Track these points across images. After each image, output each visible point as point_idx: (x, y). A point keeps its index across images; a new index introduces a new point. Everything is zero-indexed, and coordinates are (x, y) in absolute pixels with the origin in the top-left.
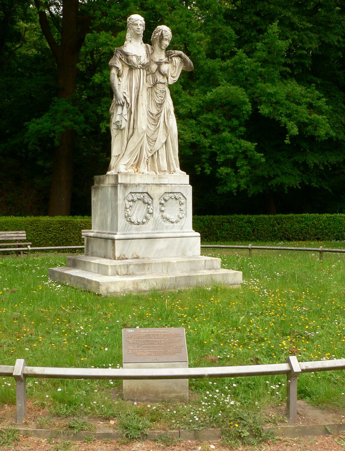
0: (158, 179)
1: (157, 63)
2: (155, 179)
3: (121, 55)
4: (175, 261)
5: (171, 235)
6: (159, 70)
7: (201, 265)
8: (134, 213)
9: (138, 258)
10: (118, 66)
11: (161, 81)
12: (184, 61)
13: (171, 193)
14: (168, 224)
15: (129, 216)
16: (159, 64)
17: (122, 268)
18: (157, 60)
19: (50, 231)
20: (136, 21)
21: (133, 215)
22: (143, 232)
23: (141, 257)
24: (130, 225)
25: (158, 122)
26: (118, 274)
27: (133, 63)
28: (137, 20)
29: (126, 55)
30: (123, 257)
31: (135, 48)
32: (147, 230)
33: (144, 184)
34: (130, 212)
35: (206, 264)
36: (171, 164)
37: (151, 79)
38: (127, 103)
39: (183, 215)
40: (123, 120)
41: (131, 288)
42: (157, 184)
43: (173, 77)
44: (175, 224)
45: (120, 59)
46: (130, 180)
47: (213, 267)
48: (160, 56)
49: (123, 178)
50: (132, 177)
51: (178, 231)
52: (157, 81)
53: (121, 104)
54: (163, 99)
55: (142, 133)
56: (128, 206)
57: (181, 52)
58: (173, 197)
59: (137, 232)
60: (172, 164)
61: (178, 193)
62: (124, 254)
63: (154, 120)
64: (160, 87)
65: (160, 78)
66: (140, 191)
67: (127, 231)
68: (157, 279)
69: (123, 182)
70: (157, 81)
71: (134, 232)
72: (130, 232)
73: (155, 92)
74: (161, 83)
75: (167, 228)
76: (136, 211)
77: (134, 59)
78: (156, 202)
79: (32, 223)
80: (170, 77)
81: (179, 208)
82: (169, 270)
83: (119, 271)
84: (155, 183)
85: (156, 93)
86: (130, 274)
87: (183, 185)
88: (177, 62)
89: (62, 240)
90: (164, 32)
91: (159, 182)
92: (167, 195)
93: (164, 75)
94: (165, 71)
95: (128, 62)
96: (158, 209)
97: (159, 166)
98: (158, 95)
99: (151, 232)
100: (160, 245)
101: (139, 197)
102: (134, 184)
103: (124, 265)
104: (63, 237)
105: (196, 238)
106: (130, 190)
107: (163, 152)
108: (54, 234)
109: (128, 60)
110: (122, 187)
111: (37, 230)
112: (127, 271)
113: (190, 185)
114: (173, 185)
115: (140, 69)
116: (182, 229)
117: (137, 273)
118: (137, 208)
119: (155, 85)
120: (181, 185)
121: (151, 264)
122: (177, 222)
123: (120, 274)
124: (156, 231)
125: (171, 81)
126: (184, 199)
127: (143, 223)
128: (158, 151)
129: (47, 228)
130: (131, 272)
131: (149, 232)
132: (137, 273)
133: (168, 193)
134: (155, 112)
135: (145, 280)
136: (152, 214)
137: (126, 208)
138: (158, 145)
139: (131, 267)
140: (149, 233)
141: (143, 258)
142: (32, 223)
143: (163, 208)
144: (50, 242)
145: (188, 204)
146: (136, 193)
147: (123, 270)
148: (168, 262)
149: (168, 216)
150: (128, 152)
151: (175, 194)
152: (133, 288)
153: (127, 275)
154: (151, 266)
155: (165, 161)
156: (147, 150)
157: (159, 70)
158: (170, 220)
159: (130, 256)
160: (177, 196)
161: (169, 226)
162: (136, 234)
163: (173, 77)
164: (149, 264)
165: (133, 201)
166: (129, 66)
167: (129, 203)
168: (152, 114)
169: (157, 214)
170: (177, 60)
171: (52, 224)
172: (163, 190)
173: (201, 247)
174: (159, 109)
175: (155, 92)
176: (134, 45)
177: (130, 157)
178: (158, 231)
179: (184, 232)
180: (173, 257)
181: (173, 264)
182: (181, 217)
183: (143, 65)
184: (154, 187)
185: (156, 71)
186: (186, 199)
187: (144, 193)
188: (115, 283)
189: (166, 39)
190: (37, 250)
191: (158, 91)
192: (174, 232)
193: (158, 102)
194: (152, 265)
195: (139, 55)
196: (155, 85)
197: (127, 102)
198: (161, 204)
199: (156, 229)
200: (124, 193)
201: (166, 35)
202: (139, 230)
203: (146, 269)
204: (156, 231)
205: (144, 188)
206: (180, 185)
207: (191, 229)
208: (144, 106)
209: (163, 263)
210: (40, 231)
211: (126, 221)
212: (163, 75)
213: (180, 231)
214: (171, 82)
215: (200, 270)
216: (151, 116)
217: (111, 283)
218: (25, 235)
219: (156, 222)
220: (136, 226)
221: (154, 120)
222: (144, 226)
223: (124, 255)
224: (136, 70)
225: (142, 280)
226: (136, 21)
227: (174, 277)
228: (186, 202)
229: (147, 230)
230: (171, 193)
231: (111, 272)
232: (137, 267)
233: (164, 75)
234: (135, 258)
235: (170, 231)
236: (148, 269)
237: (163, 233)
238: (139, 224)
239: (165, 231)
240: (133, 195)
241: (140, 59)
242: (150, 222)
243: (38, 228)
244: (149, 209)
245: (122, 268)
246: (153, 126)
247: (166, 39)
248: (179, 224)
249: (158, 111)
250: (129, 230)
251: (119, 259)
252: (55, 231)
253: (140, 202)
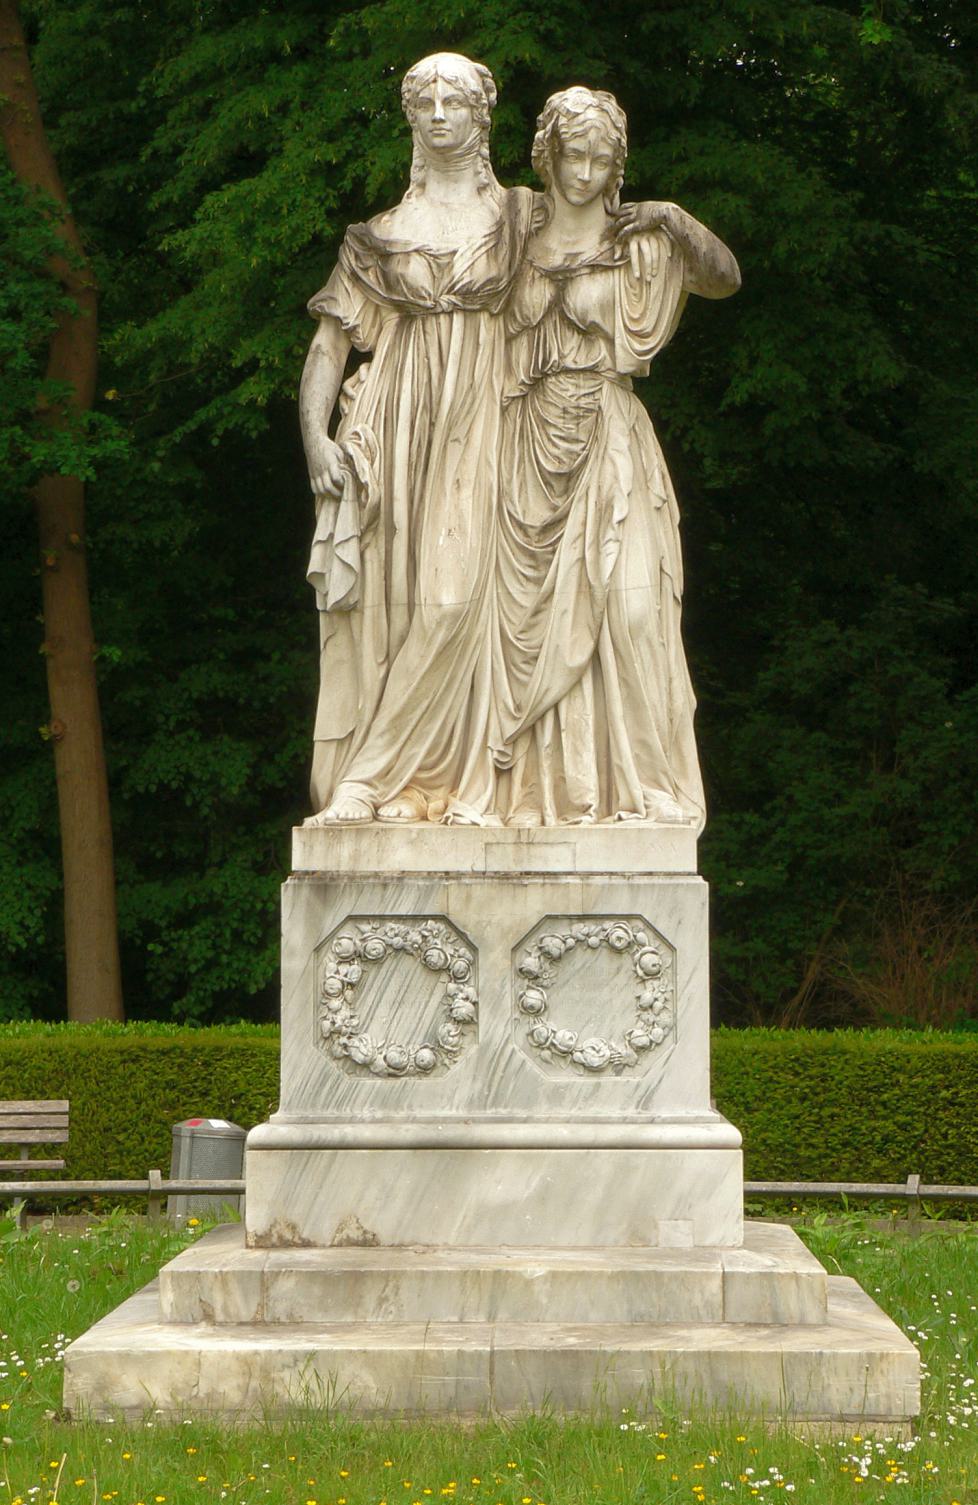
0: (510, 849)
1: (551, 275)
2: (494, 848)
3: (357, 257)
4: (540, 1271)
5: (563, 1133)
6: (557, 305)
7: (698, 1300)
8: (370, 1016)
9: (368, 1242)
10: (339, 312)
11: (569, 363)
12: (682, 246)
13: (583, 918)
14: (565, 1076)
15: (339, 1033)
16: (562, 278)
17: (233, 1286)
18: (556, 260)
19: (884, 1104)
20: (427, 84)
21: (364, 1027)
22: (420, 1113)
23: (384, 1237)
24: (347, 1080)
25: (550, 562)
26: (208, 1317)
27: (410, 288)
28: (449, 81)
29: (383, 254)
30: (288, 1235)
31: (443, 220)
32: (444, 1104)
33: (430, 875)
34: (345, 1012)
35: (732, 1295)
36: (615, 769)
37: (523, 358)
38: (360, 487)
39: (658, 1031)
40: (337, 570)
41: (231, 1391)
42: (505, 877)
43: (640, 335)
44: (608, 1079)
45: (355, 278)
46: (356, 857)
47: (775, 1314)
48: (577, 238)
49: (319, 849)
50: (365, 843)
51: (616, 1113)
52: (545, 362)
53: (328, 492)
54: (577, 447)
55: (439, 624)
56: (334, 984)
57: (668, 207)
58: (593, 940)
59: (379, 1114)
60: (621, 769)
61: (628, 917)
62: (295, 1218)
63: (532, 555)
64: (565, 390)
65: (571, 351)
66: (402, 911)
67: (326, 1106)
68: (380, 1354)
69: (317, 864)
70: (545, 362)
71: (366, 1113)
72: (347, 1112)
73: (539, 417)
74: (567, 371)
75: (557, 1095)
76: (383, 1011)
77: (417, 272)
78: (495, 961)
79: (804, 1066)
80: (621, 337)
81: (631, 998)
82: (502, 1315)
83: (218, 1300)
84: (495, 866)
85: (544, 423)
86: (277, 1322)
87: (655, 880)
88: (648, 259)
89: (939, 1155)
90: (563, 120)
91: (518, 861)
92: (563, 930)
93: (588, 332)
94: (585, 313)
95: (389, 287)
96: (508, 1001)
97: (560, 781)
98: (552, 431)
99: (462, 1113)
100: (500, 1183)
101: (398, 941)
102: (376, 875)
103: (243, 1277)
104: (945, 1136)
105: (710, 1153)
106: (346, 906)
107: (580, 713)
108: (901, 1119)
109: (390, 282)
110: (305, 892)
111: (821, 1098)
112: (261, 1306)
113: (700, 879)
114: (597, 880)
115: (450, 314)
116: (645, 1102)
117: (318, 1317)
118: (390, 995)
119: (537, 383)
120: (645, 880)
121: (399, 1275)
122: (618, 1066)
123: (220, 1317)
124: (490, 1112)
125: (631, 353)
126: (663, 950)
127: (425, 1070)
128: (556, 707)
129: (873, 1087)
130: (280, 1309)
131: (453, 1113)
132: (318, 1317)
133: (570, 918)
134: (536, 513)
135: (311, 1355)
136: (468, 1023)
137: (327, 995)
138: (547, 680)
139: (286, 1285)
140: (445, 1120)
141: (400, 1246)
142: (804, 1066)
143: (533, 997)
144: (876, 1163)
145: (682, 978)
146: (382, 918)
147: (237, 1298)
148: (497, 1273)
149: (563, 1036)
150: (382, 723)
151: (608, 925)
152: (245, 1390)
153: (260, 1324)
154: (397, 1288)
155: (589, 758)
156: (501, 706)
157: (557, 305)
158: (578, 1055)
159: (326, 1231)
160: (619, 933)
161: (567, 1086)
162: (374, 1121)
163: (640, 335)
164: (386, 1276)
165: (359, 956)
166: (399, 306)
167: (344, 969)
168: (521, 526)
169: (497, 1026)
170: (650, 250)
171: (900, 1070)
172: (533, 903)
173: (750, 1197)
174: (559, 502)
175: (539, 417)
176: (432, 202)
177: (391, 743)
178: (503, 1112)
179: (652, 1121)
180: (574, 1248)
181: (529, 1283)
182: (644, 1041)
183: (467, 293)
184: (480, 891)
185: (548, 312)
186: (672, 948)
187: (426, 918)
188: (149, 1359)
189: (580, 155)
190: (805, 1196)
191: (552, 415)
192: (596, 1121)
193: (550, 467)
194: (405, 1284)
195: (436, 244)
196: (537, 383)
197: (356, 477)
198: (523, 973)
199: (495, 1104)
200: (313, 921)
201: (575, 136)
202: (398, 1105)
203: (370, 1300)
204: (490, 1112)
205: (428, 892)
206: (638, 880)
207: (706, 1109)
208: (467, 492)
209: (470, 1277)
210: (833, 1102)
211: (326, 1059)
212: (581, 332)
213: (631, 1112)
214: (625, 363)
215: (688, 1326)
216: (519, 538)
217: (125, 1358)
218: (64, 1121)
219: (492, 1064)
220: (379, 1082)
221: (532, 555)
222: (424, 1083)
223: (293, 1228)
224: (431, 323)
225: (296, 1357)
226: (427, 84)
227: (479, 1354)
228: (673, 965)
229: (444, 1104)
230: (583, 918)
231: (175, 1306)
232: (317, 1290)
233: (588, 332)
234: (351, 1243)
235: (574, 1112)
236: (382, 1300)
237: (525, 1121)
238: (395, 1071)
239: (541, 1111)
240: (366, 927)
241: (450, 265)
242: (459, 1068)
243: (826, 1090)
244: (453, 997)
245: (233, 1286)
246: (531, 587)
247: (580, 155)
248: (629, 1078)
249: (555, 508)
250: (339, 1105)
251: (263, 1242)
252: (911, 1105)
253: (408, 964)
